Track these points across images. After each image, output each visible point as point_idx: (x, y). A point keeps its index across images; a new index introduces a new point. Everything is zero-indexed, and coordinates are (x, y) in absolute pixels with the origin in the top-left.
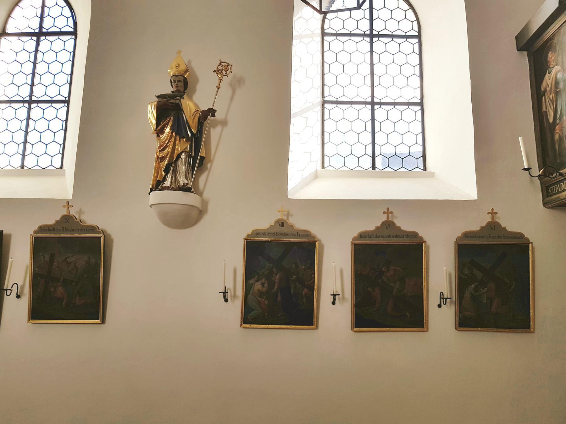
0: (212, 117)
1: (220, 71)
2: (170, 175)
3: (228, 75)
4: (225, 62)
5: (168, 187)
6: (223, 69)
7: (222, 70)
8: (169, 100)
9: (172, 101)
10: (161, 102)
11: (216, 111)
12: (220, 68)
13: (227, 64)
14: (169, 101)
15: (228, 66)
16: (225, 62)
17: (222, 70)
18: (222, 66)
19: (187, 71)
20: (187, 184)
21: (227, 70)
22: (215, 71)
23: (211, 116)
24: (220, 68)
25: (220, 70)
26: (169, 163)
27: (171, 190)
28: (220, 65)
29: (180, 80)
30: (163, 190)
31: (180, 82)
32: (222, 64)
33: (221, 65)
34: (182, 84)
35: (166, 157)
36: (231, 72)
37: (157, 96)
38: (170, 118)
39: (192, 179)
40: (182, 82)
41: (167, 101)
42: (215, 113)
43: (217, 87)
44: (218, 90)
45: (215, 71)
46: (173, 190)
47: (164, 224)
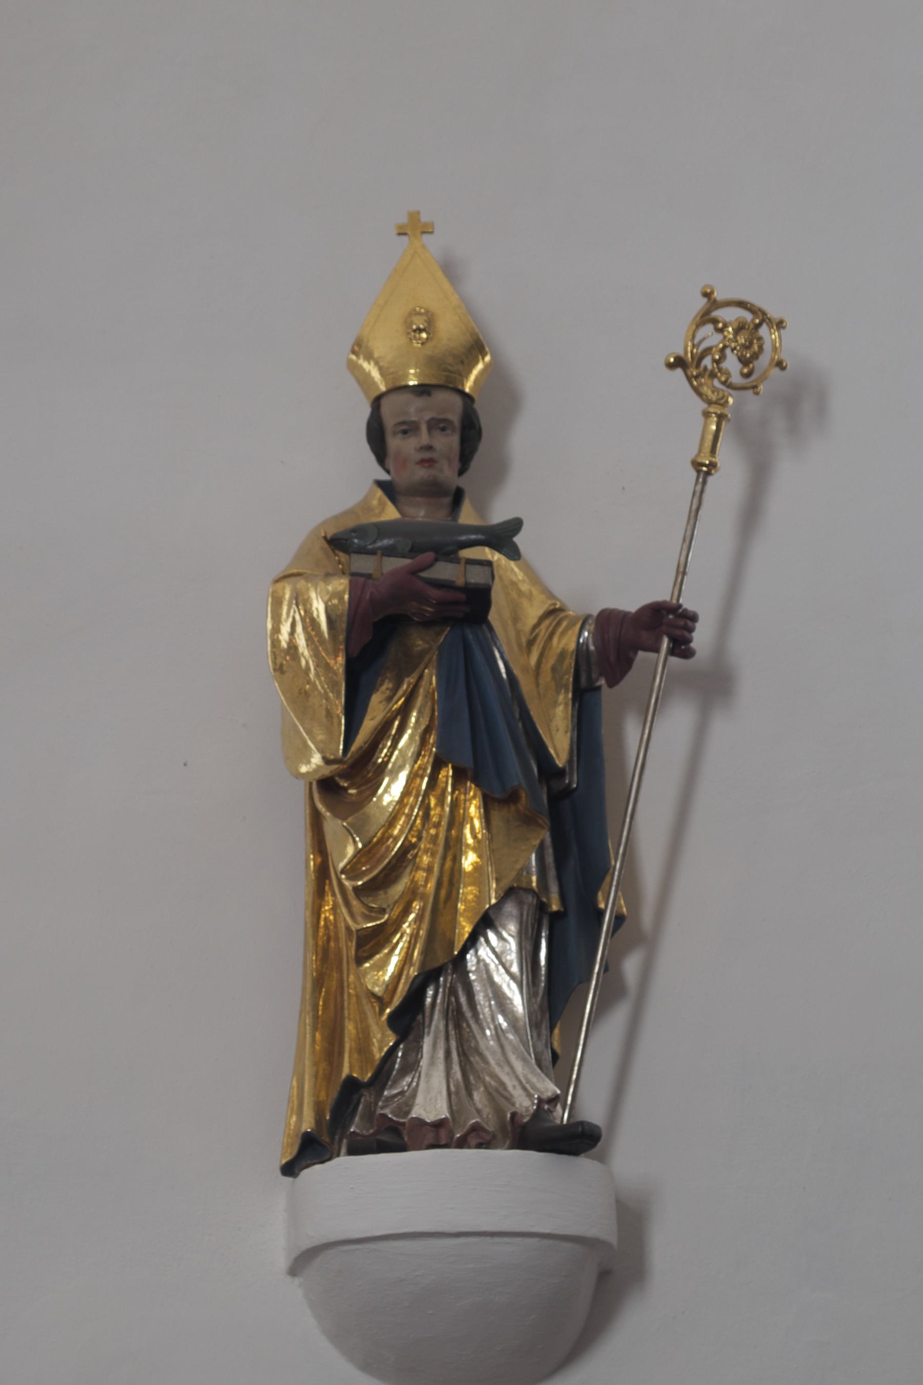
0: (673, 660)
1: (707, 362)
2: (434, 1045)
3: (761, 388)
4: (741, 304)
5: (439, 1125)
6: (725, 347)
7: (722, 350)
8: (423, 569)
9: (444, 571)
10: (369, 576)
11: (693, 618)
12: (709, 337)
13: (748, 316)
14: (424, 574)
15: (757, 326)
16: (741, 304)
17: (722, 350)
18: (721, 331)
19: (476, 348)
20: (554, 1100)
21: (755, 356)
22: (679, 363)
23: (672, 652)
24: (709, 337)
25: (708, 351)
26: (428, 968)
27: (462, 1144)
28: (706, 318)
29: (445, 420)
30: (402, 1148)
31: (443, 429)
32: (718, 313)
33: (715, 321)
34: (449, 442)
35: (396, 925)
36: (780, 365)
37: (329, 536)
38: (421, 677)
39: (530, 1055)
40: (454, 430)
41: (414, 572)
42: (691, 630)
43: (697, 465)
44: (704, 482)
45: (679, 363)
46: (474, 1142)
47: (366, 1367)
